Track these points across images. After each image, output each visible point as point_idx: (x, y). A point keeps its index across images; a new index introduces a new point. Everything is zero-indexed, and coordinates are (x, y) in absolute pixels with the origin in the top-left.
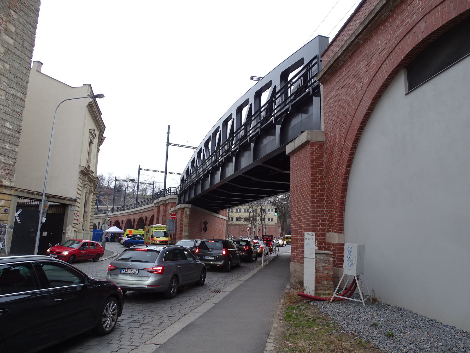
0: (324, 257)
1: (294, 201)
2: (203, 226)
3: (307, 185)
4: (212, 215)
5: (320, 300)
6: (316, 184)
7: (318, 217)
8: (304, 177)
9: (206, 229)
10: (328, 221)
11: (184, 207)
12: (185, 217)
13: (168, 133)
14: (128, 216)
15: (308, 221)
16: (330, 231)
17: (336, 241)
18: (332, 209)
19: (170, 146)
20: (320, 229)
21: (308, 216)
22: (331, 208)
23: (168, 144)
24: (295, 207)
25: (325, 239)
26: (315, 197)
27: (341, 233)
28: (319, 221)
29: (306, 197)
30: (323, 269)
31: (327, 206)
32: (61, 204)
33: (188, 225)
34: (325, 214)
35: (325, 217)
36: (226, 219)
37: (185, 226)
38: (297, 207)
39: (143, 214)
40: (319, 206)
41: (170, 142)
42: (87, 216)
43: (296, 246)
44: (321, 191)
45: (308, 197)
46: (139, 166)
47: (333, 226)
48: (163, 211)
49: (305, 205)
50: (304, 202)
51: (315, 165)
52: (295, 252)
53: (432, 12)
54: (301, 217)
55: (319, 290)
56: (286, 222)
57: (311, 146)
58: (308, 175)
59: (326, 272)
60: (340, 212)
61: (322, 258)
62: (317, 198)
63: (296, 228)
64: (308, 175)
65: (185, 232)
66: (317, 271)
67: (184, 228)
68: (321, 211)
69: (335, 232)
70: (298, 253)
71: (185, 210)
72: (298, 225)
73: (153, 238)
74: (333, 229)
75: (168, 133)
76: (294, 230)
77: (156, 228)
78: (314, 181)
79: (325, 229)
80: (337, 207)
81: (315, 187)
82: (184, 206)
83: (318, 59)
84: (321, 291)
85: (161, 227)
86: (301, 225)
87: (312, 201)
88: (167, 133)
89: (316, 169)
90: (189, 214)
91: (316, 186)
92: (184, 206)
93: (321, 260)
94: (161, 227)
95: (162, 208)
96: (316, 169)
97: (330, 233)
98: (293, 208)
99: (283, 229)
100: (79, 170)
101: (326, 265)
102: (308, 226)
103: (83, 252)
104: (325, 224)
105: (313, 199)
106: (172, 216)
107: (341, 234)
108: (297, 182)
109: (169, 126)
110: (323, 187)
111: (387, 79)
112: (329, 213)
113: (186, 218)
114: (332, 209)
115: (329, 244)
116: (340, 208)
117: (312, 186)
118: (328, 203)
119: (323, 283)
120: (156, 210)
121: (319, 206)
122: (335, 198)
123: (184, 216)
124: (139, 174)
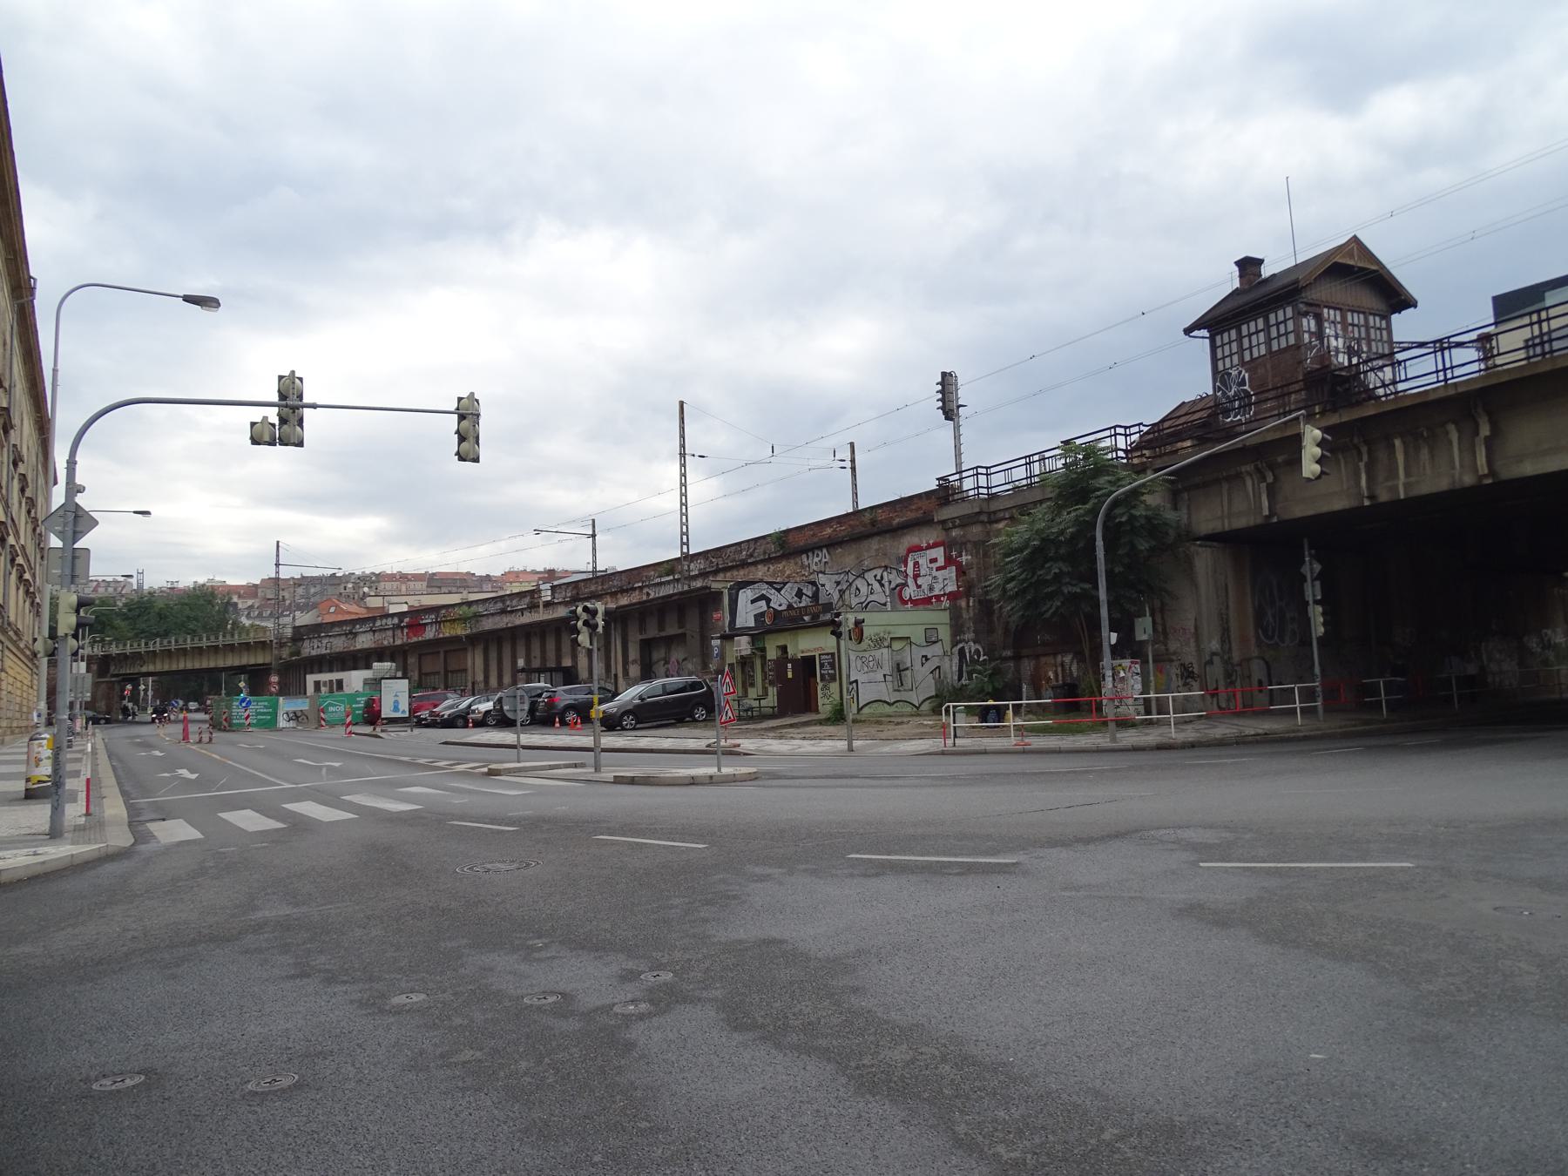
109: (682, 404)
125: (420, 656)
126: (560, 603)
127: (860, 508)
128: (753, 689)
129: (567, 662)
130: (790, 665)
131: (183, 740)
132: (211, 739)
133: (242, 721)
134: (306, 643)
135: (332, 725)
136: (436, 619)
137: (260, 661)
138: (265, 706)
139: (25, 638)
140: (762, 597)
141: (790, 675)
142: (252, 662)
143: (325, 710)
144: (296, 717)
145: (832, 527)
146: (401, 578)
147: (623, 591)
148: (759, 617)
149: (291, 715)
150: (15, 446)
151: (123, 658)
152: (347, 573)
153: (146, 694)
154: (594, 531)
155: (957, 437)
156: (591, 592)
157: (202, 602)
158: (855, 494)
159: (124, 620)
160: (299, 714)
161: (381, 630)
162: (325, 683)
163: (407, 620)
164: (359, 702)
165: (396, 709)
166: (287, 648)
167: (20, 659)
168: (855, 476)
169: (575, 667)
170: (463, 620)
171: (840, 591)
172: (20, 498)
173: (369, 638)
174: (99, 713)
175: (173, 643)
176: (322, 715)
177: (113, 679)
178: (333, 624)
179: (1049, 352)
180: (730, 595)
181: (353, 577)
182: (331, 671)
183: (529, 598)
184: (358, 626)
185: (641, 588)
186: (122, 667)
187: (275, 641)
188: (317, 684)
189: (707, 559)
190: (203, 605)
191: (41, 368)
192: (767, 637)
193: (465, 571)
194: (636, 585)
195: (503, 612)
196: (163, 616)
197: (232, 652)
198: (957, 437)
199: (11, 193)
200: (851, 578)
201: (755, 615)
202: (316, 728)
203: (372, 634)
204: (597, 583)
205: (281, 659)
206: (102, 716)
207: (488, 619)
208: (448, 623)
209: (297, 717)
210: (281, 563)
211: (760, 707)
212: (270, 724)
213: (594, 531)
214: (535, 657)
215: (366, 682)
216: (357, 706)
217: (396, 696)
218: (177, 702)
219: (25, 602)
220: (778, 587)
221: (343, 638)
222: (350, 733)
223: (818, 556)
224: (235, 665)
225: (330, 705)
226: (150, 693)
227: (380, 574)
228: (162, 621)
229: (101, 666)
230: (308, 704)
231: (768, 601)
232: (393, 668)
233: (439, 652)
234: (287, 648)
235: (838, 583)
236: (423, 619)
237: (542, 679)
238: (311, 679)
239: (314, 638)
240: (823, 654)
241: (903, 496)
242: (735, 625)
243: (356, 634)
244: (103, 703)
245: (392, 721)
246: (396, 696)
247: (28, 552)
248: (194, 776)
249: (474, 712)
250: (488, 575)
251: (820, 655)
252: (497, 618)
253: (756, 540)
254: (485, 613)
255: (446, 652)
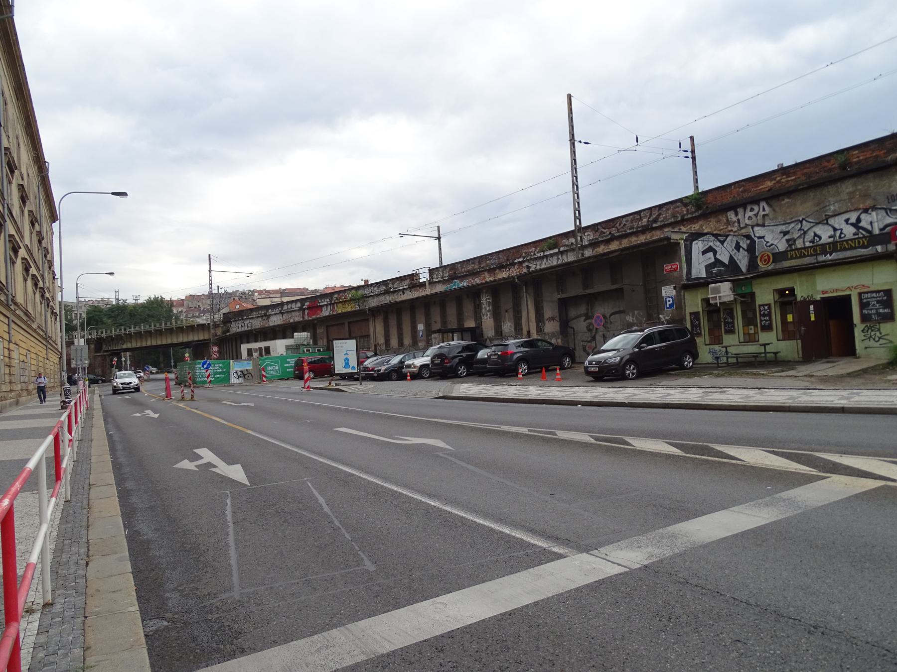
109: (569, 97)
125: (327, 327)
126: (438, 282)
127: (583, 226)
128: (731, 336)
129: (470, 324)
130: (812, 307)
131: (167, 397)
132: (192, 397)
133: (204, 379)
134: (233, 324)
135: (270, 380)
136: (331, 301)
137: (202, 338)
138: (220, 367)
139: (38, 320)
140: (710, 249)
141: (813, 318)
142: (196, 339)
143: (265, 370)
144: (243, 375)
145: (775, 179)
146: (266, 292)
147: (501, 267)
148: (708, 267)
149: (240, 374)
150: (44, 248)
151: (111, 340)
152: (234, 291)
153: (126, 363)
154: (439, 235)
155: (440, 245)
156: (469, 271)
157: (155, 305)
158: (696, 181)
159: (109, 318)
160: (245, 373)
161: (287, 312)
162: (256, 350)
163: (307, 304)
164: (288, 363)
165: (347, 365)
166: (220, 328)
167: (29, 334)
168: (695, 164)
169: (479, 326)
170: (353, 300)
171: (788, 241)
172: (30, 229)
173: (279, 319)
174: (98, 376)
175: (143, 328)
176: (263, 373)
177: (105, 354)
178: (252, 310)
179: (771, 89)
180: (686, 246)
181: (238, 293)
182: (256, 341)
183: (409, 280)
184: (270, 311)
185: (520, 263)
186: (110, 346)
187: (211, 324)
188: (250, 352)
189: (596, 231)
190: (156, 308)
191: (29, 90)
192: (754, 282)
193: (302, 287)
194: (517, 261)
195: (387, 292)
196: (132, 315)
197: (182, 333)
198: (440, 245)
199: (27, 99)
200: (806, 226)
201: (706, 267)
202: (260, 383)
203: (281, 315)
204: (473, 263)
205: (216, 335)
206: (100, 378)
207: (374, 298)
208: (340, 305)
209: (244, 375)
210: (212, 270)
211: (765, 353)
212: (225, 380)
213: (439, 235)
214: (436, 322)
215: (288, 348)
216: (287, 365)
217: (346, 354)
218: (148, 368)
219: (51, 318)
220: (721, 239)
221: (260, 319)
222: (309, 387)
223: (752, 210)
224: (184, 341)
225: (267, 365)
226: (128, 363)
227: (254, 290)
228: (132, 318)
229: (96, 345)
230: (251, 365)
231: (715, 252)
232: (309, 336)
233: (344, 323)
234: (220, 328)
235: (785, 233)
236: (319, 303)
237: (455, 338)
238: (244, 347)
239: (239, 320)
240: (865, 293)
241: (798, 162)
242: (691, 276)
243: (269, 316)
244: (100, 369)
245: (344, 377)
246: (346, 354)
247: (14, 214)
248: (156, 416)
249: (409, 366)
250: (316, 290)
251: (860, 294)
252: (381, 298)
253: (660, 207)
254: (372, 294)
255: (349, 323)
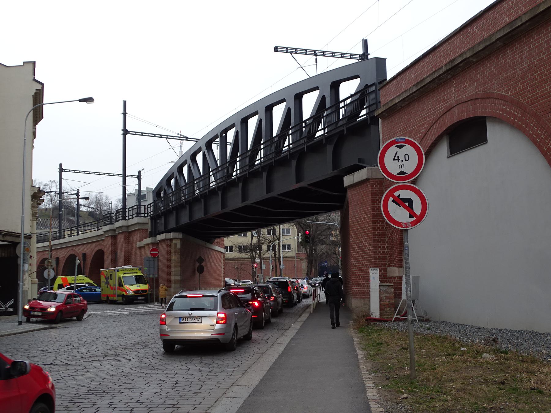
0: (387, 289)
1: (354, 236)
2: (197, 265)
3: (368, 222)
4: (207, 248)
5: (384, 321)
6: (377, 221)
7: (380, 253)
8: (365, 213)
9: (201, 270)
10: (389, 257)
11: (172, 237)
12: (175, 252)
13: (125, 114)
14: (43, 253)
15: (370, 257)
16: (391, 266)
17: (397, 275)
18: (392, 245)
19: (128, 135)
20: (382, 264)
21: (370, 252)
22: (391, 244)
23: (126, 132)
24: (355, 243)
25: (386, 273)
26: (377, 234)
27: (401, 267)
28: (380, 257)
29: (367, 234)
30: (386, 298)
31: (388, 242)
32: (11, 243)
33: (179, 264)
34: (386, 249)
35: (385, 243)
36: (223, 252)
37: (175, 267)
38: (358, 243)
39: (75, 249)
40: (380, 242)
41: (128, 128)
42: (31, 257)
43: (358, 282)
44: (381, 228)
45: (369, 234)
46: (61, 165)
47: (394, 261)
48: (125, 243)
49: (366, 241)
50: (366, 238)
51: (375, 202)
52: (357, 288)
53: (461, 104)
54: (362, 253)
55: (383, 315)
56: (315, 250)
57: (371, 184)
58: (369, 212)
59: (388, 300)
60: (399, 248)
61: (385, 289)
62: (378, 235)
63: (357, 263)
64: (369, 212)
65: (175, 275)
66: (381, 300)
67: (173, 269)
68: (382, 247)
69: (395, 266)
70: (361, 288)
71: (174, 242)
72: (360, 261)
73: (123, 287)
74: (393, 263)
75: (125, 114)
76: (355, 266)
77: (125, 272)
78: (375, 218)
79: (386, 264)
80: (397, 243)
81: (376, 224)
82: (171, 235)
83: (376, 88)
84: (385, 316)
85: (131, 270)
86: (363, 261)
87: (374, 237)
88: (123, 114)
89: (376, 207)
90: (180, 248)
91: (377, 223)
92: (173, 237)
93: (384, 291)
94: (131, 270)
95: (121, 239)
96: (376, 207)
97: (391, 267)
98: (354, 243)
99: (312, 263)
100: (31, 192)
101: (388, 295)
102: (370, 262)
103: (69, 307)
104: (386, 259)
105: (374, 236)
106: (152, 252)
107: (401, 268)
108: (357, 218)
109: (125, 103)
110: (383, 223)
111: (434, 141)
112: (389, 249)
113: (177, 254)
114: (392, 245)
115: (390, 278)
116: (400, 244)
117: (373, 218)
118: (389, 239)
119: (386, 310)
120: (108, 243)
121: (380, 242)
122: (395, 235)
123: (172, 250)
124: (61, 179)
